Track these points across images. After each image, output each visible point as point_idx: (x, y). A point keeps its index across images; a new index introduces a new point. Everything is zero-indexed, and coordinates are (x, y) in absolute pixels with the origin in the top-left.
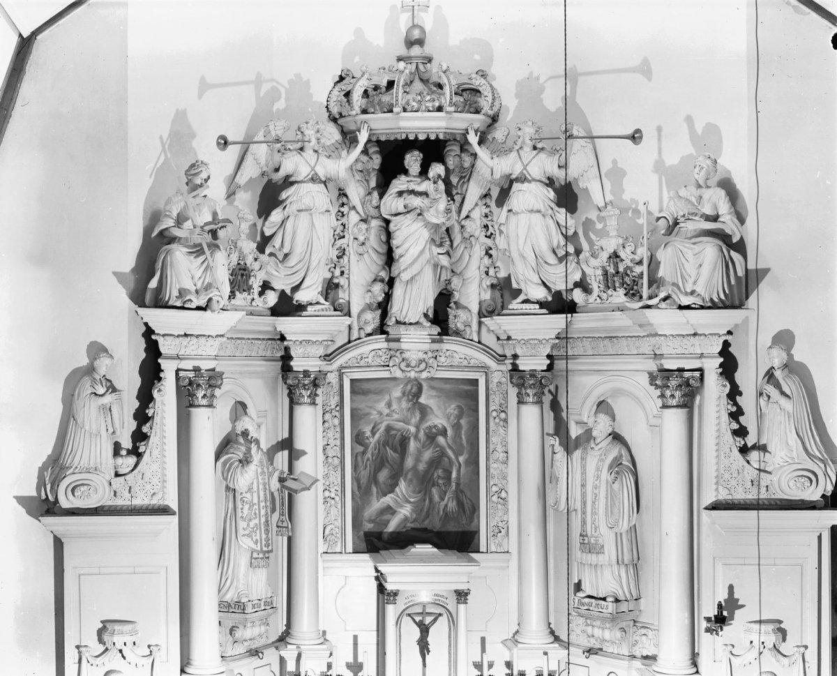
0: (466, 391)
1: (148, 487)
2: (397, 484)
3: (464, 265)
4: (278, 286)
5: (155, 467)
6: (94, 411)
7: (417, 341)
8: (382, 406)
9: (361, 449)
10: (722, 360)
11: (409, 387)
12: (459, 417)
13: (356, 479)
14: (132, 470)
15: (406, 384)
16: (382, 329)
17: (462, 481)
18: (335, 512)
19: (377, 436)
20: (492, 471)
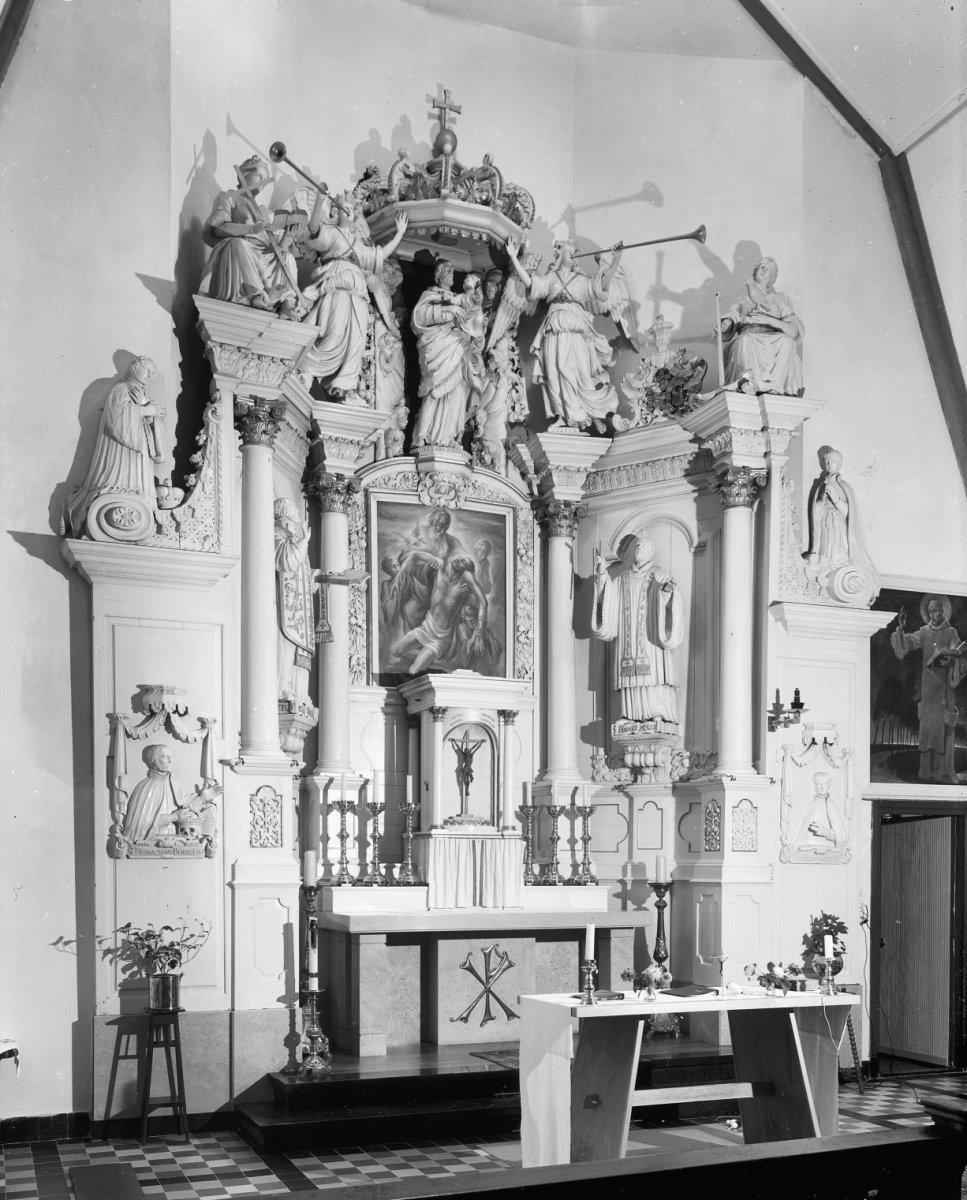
0: (494, 527)
1: (200, 528)
3: (490, 398)
5: (209, 504)
7: (449, 461)
8: (409, 533)
9: (388, 577)
11: (436, 517)
12: (487, 553)
13: (383, 609)
14: (180, 505)
15: (434, 514)
16: (408, 449)
17: (488, 620)
19: (404, 565)
20: (519, 610)
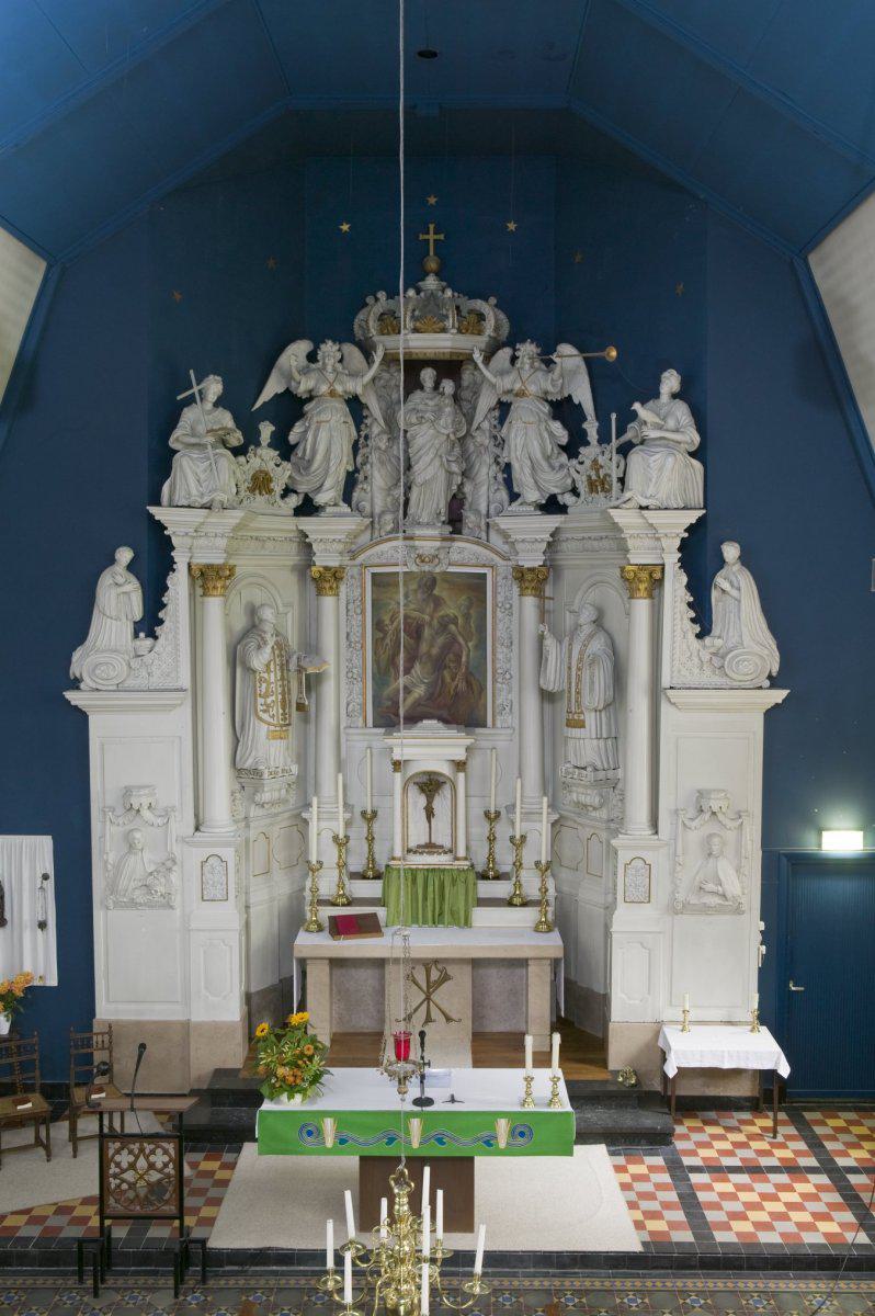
2: (412, 667)
4: (302, 488)
6: (113, 596)
7: (429, 538)
10: (680, 555)
12: (469, 608)
13: (376, 661)
18: (357, 687)
